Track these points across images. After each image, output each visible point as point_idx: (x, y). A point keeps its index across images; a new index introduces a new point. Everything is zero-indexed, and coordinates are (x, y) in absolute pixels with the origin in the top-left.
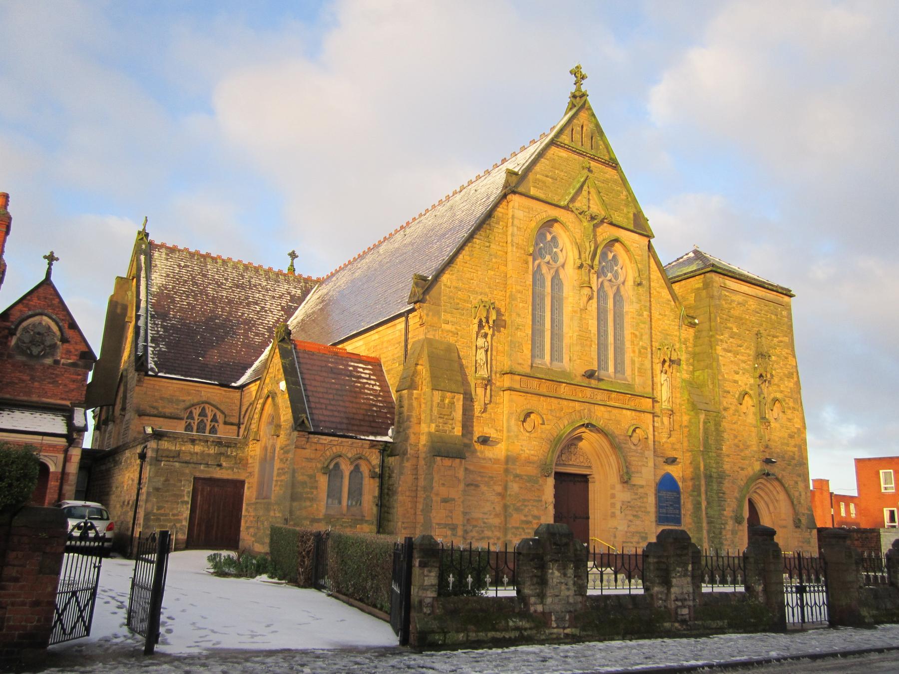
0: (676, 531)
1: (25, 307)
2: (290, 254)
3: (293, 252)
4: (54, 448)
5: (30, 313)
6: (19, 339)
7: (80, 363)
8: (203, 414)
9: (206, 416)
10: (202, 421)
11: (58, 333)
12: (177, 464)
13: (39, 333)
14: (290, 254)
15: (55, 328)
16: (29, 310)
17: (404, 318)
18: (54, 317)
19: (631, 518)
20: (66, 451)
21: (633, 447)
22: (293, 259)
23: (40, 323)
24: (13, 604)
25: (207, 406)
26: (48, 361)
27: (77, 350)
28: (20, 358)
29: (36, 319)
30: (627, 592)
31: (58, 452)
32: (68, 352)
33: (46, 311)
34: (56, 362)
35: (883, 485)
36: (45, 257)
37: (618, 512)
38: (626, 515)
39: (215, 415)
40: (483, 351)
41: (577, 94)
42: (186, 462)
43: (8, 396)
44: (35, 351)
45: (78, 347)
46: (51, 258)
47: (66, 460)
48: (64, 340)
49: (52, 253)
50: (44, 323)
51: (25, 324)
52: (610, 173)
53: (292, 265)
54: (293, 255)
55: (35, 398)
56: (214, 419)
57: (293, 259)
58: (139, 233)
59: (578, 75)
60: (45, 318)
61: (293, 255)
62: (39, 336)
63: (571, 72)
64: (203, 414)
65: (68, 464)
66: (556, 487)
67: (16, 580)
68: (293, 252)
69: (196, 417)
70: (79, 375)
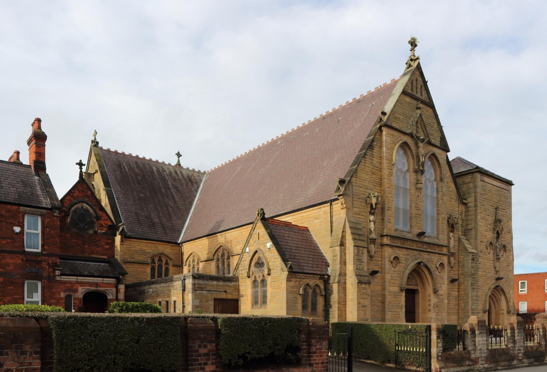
0: (234, 318)
1: (71, 197)
2: (177, 154)
3: (179, 153)
4: (109, 284)
5: (75, 201)
6: (71, 218)
7: (109, 232)
8: (160, 260)
9: (162, 261)
10: (160, 264)
11: (94, 214)
12: (205, 292)
13: (82, 214)
14: (177, 154)
15: (91, 211)
16: (74, 199)
17: (329, 204)
18: (90, 203)
19: (437, 311)
20: (117, 287)
21: (439, 274)
22: (179, 158)
23: (82, 207)
24: (316, 364)
25: (162, 255)
26: (91, 232)
27: (106, 224)
28: (74, 230)
29: (79, 205)
30: (498, 347)
31: (112, 287)
32: (101, 226)
33: (84, 200)
34: (96, 232)
35: (520, 289)
36: (77, 164)
37: (432, 309)
39: (167, 261)
40: (372, 222)
41: (413, 57)
42: (209, 291)
43: (71, 254)
44: (82, 225)
45: (106, 222)
46: (497, 209)
47: (118, 291)
48: (98, 218)
49: (81, 161)
50: (84, 207)
51: (73, 208)
52: (427, 111)
53: (179, 161)
54: (179, 155)
55: (87, 255)
56: (167, 263)
57: (179, 158)
58: (92, 142)
59: (413, 44)
60: (85, 204)
61: (179, 155)
62: (83, 215)
63: (409, 42)
64: (160, 260)
65: (119, 294)
66: (406, 296)
67: (315, 353)
68: (179, 153)
69: (157, 262)
70: (110, 240)
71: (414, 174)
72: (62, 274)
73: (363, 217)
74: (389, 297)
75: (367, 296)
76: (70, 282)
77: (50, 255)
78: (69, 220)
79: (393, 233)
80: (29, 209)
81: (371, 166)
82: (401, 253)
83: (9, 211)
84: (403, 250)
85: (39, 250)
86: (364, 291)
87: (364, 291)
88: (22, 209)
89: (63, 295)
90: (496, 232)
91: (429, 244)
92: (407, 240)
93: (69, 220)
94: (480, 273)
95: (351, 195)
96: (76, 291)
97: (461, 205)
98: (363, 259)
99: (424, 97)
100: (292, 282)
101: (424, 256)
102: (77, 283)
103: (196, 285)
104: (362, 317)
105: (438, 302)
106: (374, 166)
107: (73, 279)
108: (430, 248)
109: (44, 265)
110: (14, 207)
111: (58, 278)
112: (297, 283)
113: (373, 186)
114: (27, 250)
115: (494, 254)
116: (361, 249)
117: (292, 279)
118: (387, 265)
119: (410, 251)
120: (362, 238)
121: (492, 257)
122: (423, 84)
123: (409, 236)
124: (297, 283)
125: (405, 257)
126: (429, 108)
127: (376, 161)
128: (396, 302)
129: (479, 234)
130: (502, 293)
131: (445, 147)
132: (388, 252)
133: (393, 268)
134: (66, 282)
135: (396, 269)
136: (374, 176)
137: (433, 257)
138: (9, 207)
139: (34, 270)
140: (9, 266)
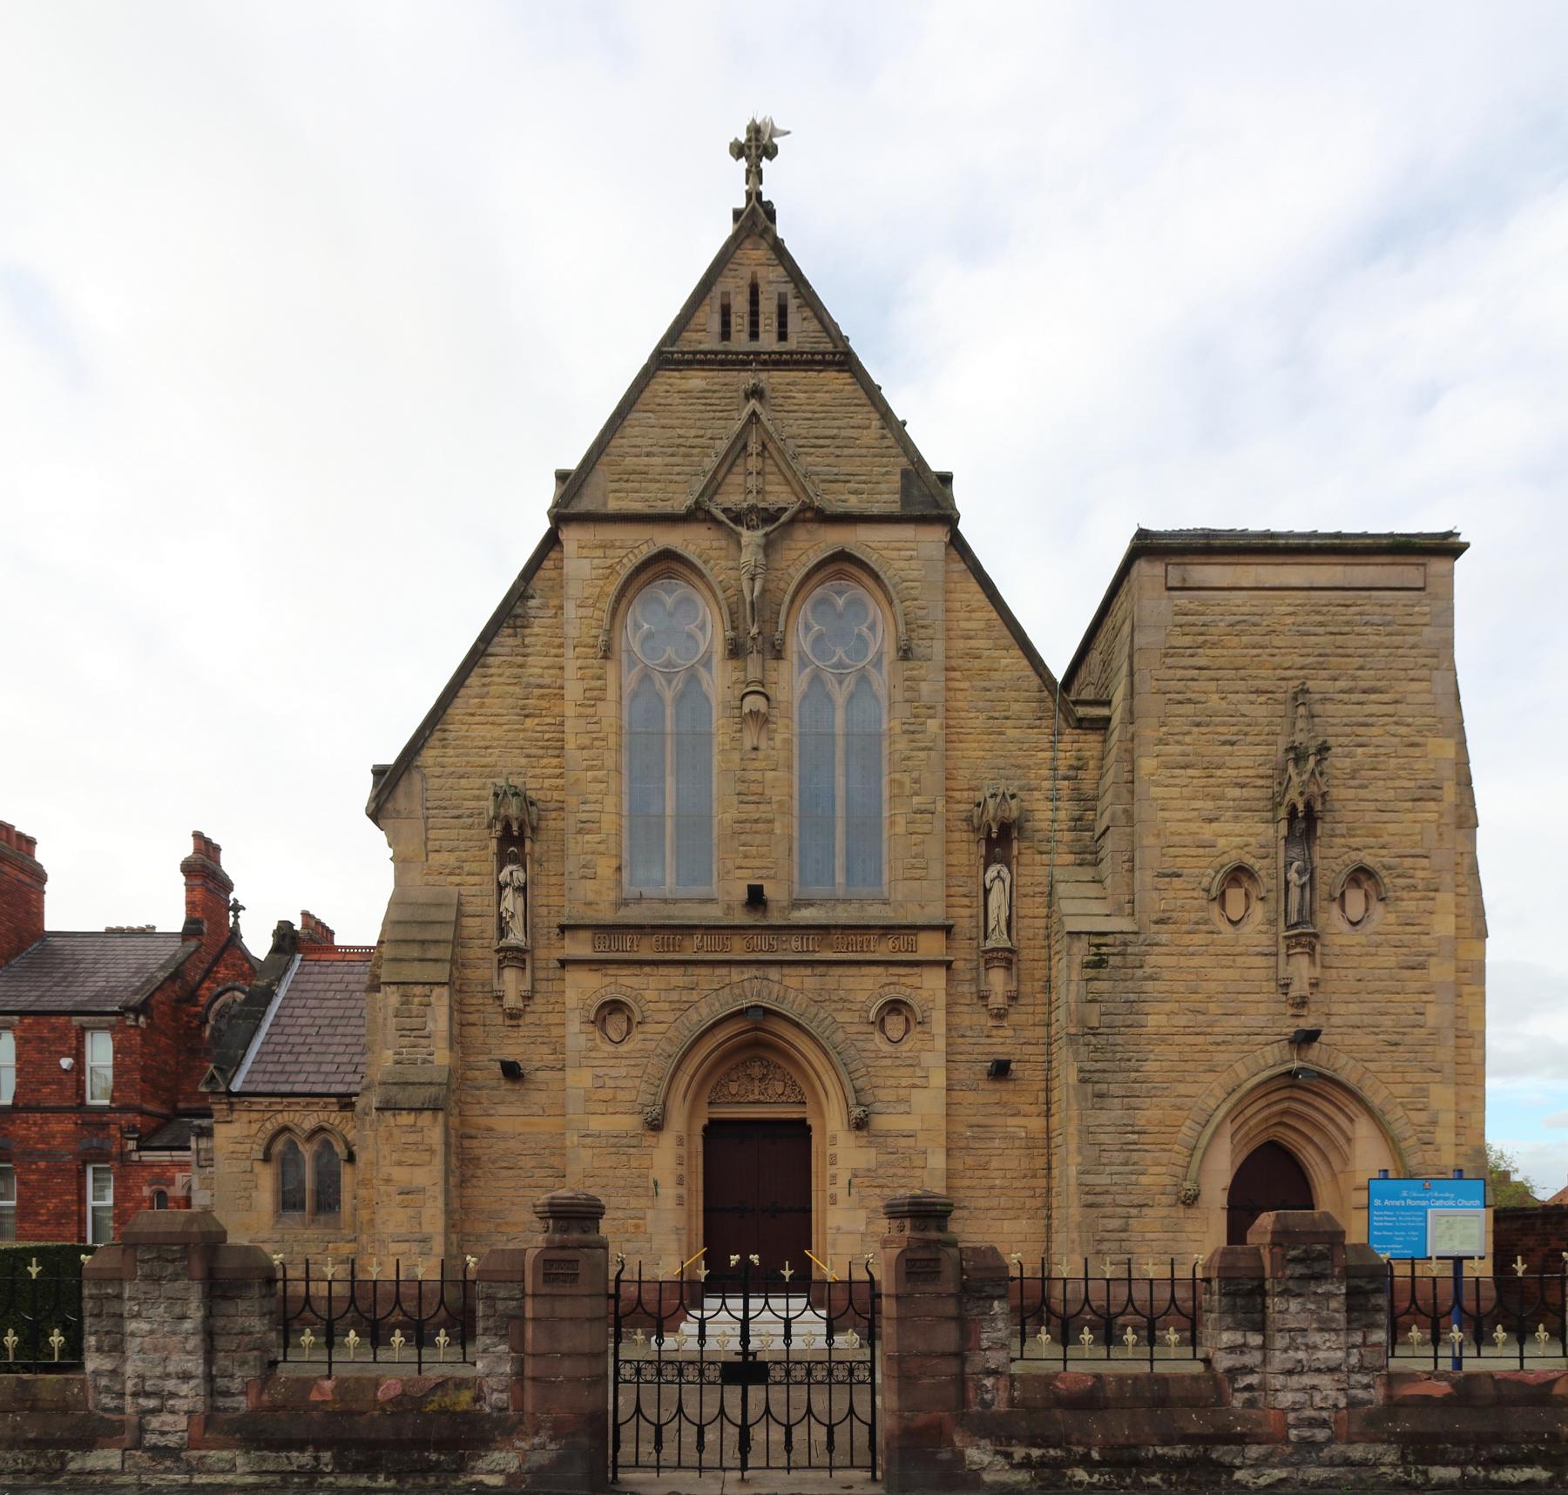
21: (886, 1048)
38: (862, 1198)
51: (217, 1005)
71: (731, 664)
72: (139, 1149)
73: (476, 879)
74: (586, 1154)
75: (426, 1157)
76: (159, 1165)
77: (123, 1109)
78: (207, 1033)
79: (607, 916)
80: (86, 1018)
81: (517, 689)
82: (624, 984)
83: (53, 1029)
84: (663, 970)
85: (89, 1102)
86: (412, 1138)
87: (412, 1138)
88: (76, 1020)
89: (146, 1191)
90: (1283, 813)
91: (825, 929)
92: (689, 929)
93: (207, 1033)
94: (1152, 1020)
95: (419, 812)
96: (172, 1182)
97: (1069, 735)
98: (431, 1026)
99: (801, 333)
100: (236, 1126)
101: (787, 981)
102: (173, 1164)
103: (202, 1154)
104: (403, 1230)
105: (880, 1165)
106: (528, 685)
107: (164, 1156)
108: (830, 947)
109: (114, 1131)
110: (63, 1019)
111: (135, 1157)
112: (256, 1126)
113: (523, 761)
114: (89, 1102)
115: (1272, 922)
116: (418, 990)
117: (235, 1115)
118: (576, 1034)
119: (704, 971)
120: (433, 953)
121: (1265, 940)
122: (789, 289)
123: (714, 914)
124: (256, 1126)
125: (674, 996)
126: (831, 374)
127: (537, 666)
128: (619, 1173)
129: (1149, 840)
130: (1353, 1108)
131: (938, 506)
132: (584, 989)
133: (609, 1048)
134: (152, 1165)
135: (623, 1048)
136: (529, 722)
137: (849, 983)
138: (53, 1020)
139: (95, 1142)
140: (54, 1137)
